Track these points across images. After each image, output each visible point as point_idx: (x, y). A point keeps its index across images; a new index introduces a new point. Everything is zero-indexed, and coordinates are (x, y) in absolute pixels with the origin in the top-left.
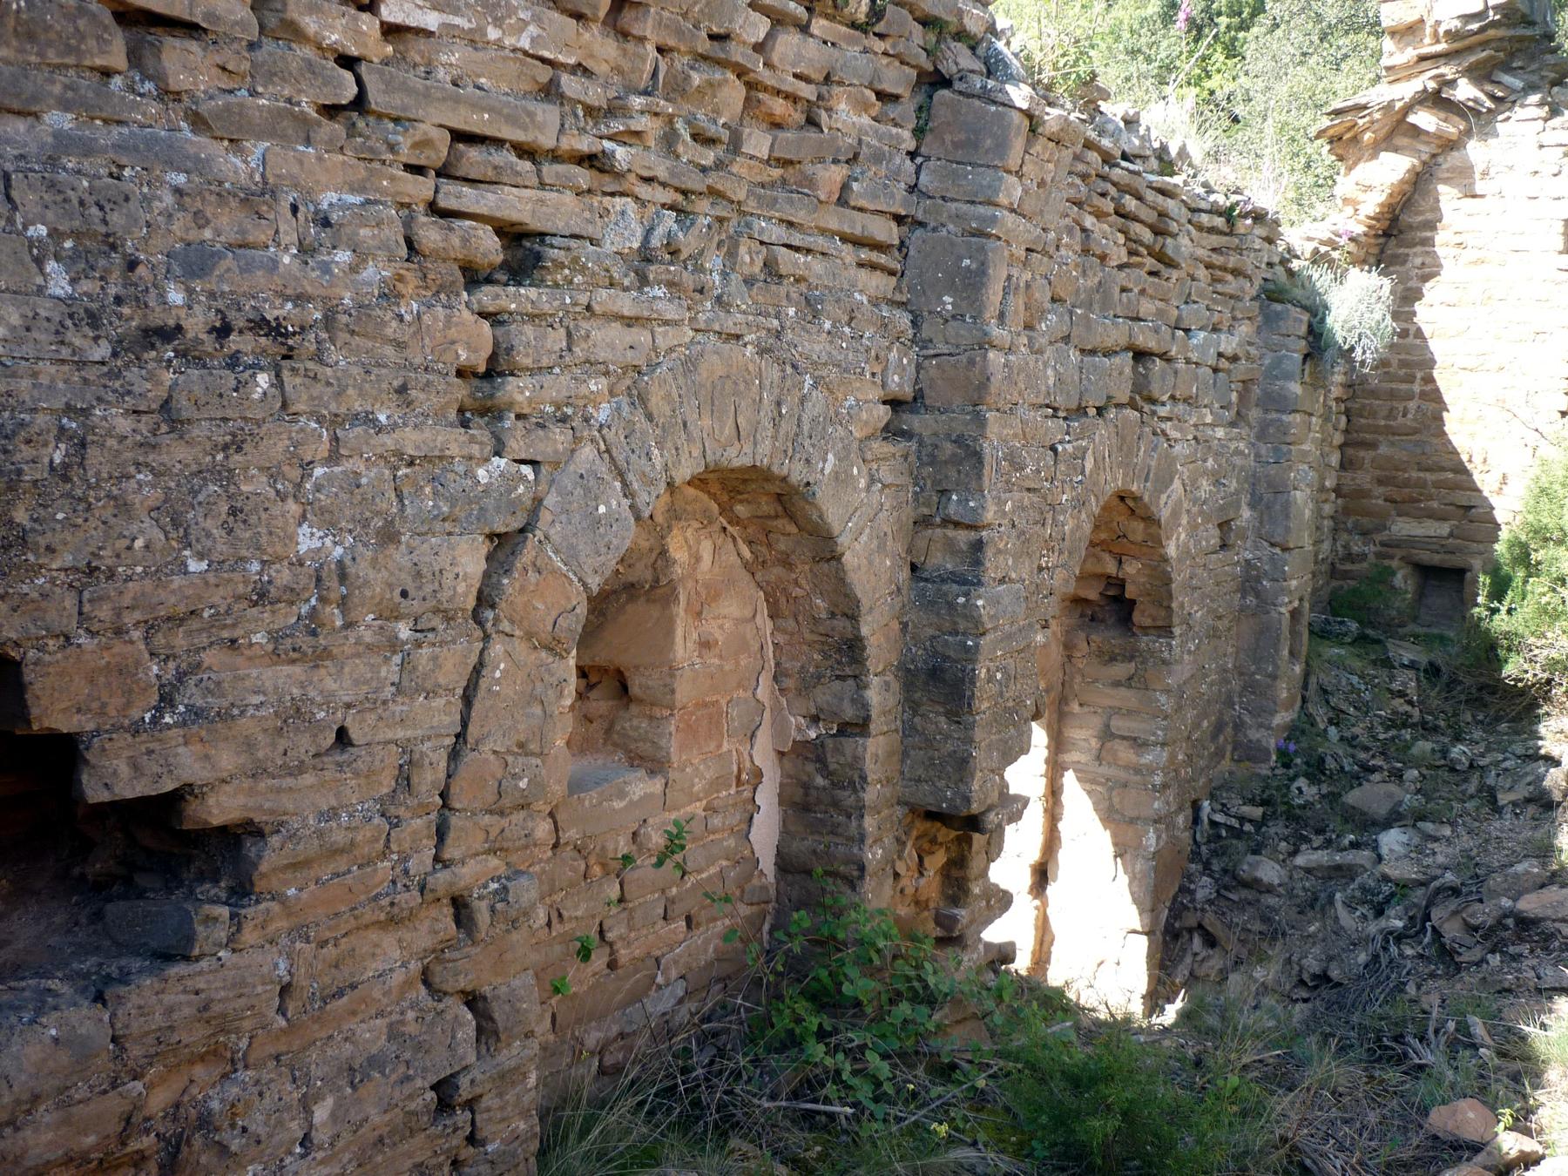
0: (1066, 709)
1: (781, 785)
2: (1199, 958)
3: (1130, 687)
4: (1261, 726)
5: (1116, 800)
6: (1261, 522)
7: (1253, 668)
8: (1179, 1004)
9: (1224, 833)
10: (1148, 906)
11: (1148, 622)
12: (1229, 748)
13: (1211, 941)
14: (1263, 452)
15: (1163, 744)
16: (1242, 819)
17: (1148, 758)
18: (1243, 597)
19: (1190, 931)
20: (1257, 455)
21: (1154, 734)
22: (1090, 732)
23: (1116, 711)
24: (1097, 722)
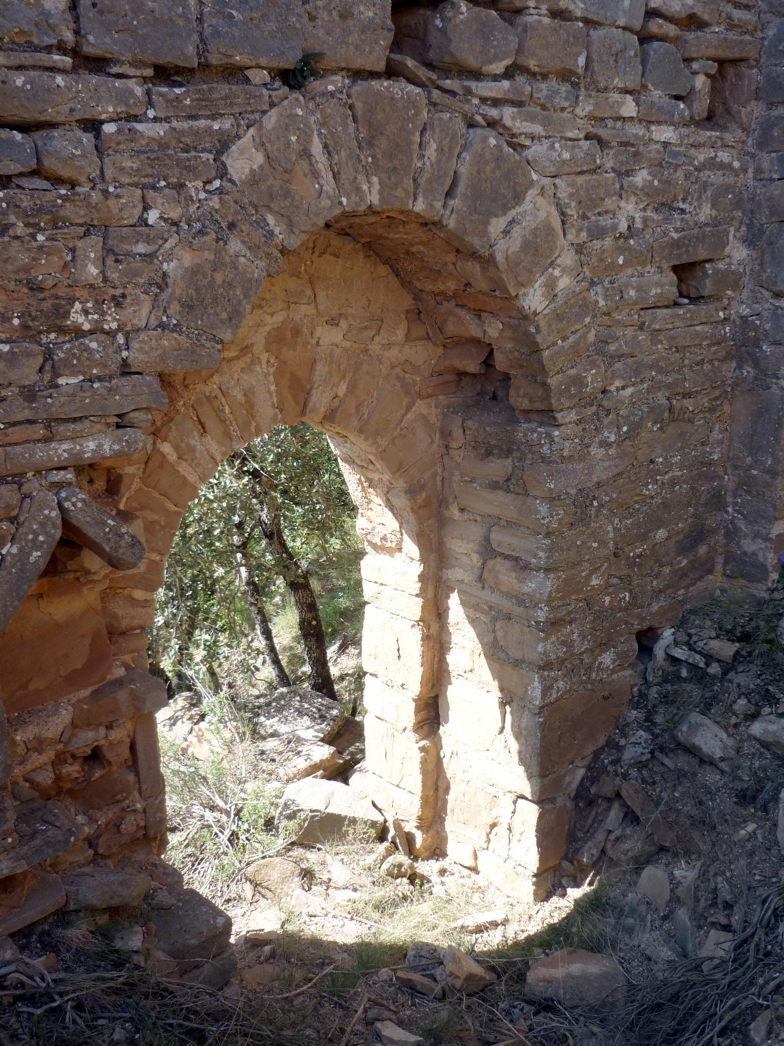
0: (447, 513)
1: (359, 570)
2: (612, 837)
3: (508, 491)
4: (757, 535)
5: (500, 634)
6: (761, 264)
7: (749, 460)
8: (585, 889)
9: (684, 673)
10: (535, 769)
11: (525, 404)
12: (720, 560)
13: (631, 817)
14: (765, 165)
15: (547, 570)
16: (709, 658)
17: (530, 586)
18: (740, 367)
19: (609, 800)
20: (758, 171)
21: (535, 556)
22: (471, 545)
23: (493, 522)
24: (477, 531)
